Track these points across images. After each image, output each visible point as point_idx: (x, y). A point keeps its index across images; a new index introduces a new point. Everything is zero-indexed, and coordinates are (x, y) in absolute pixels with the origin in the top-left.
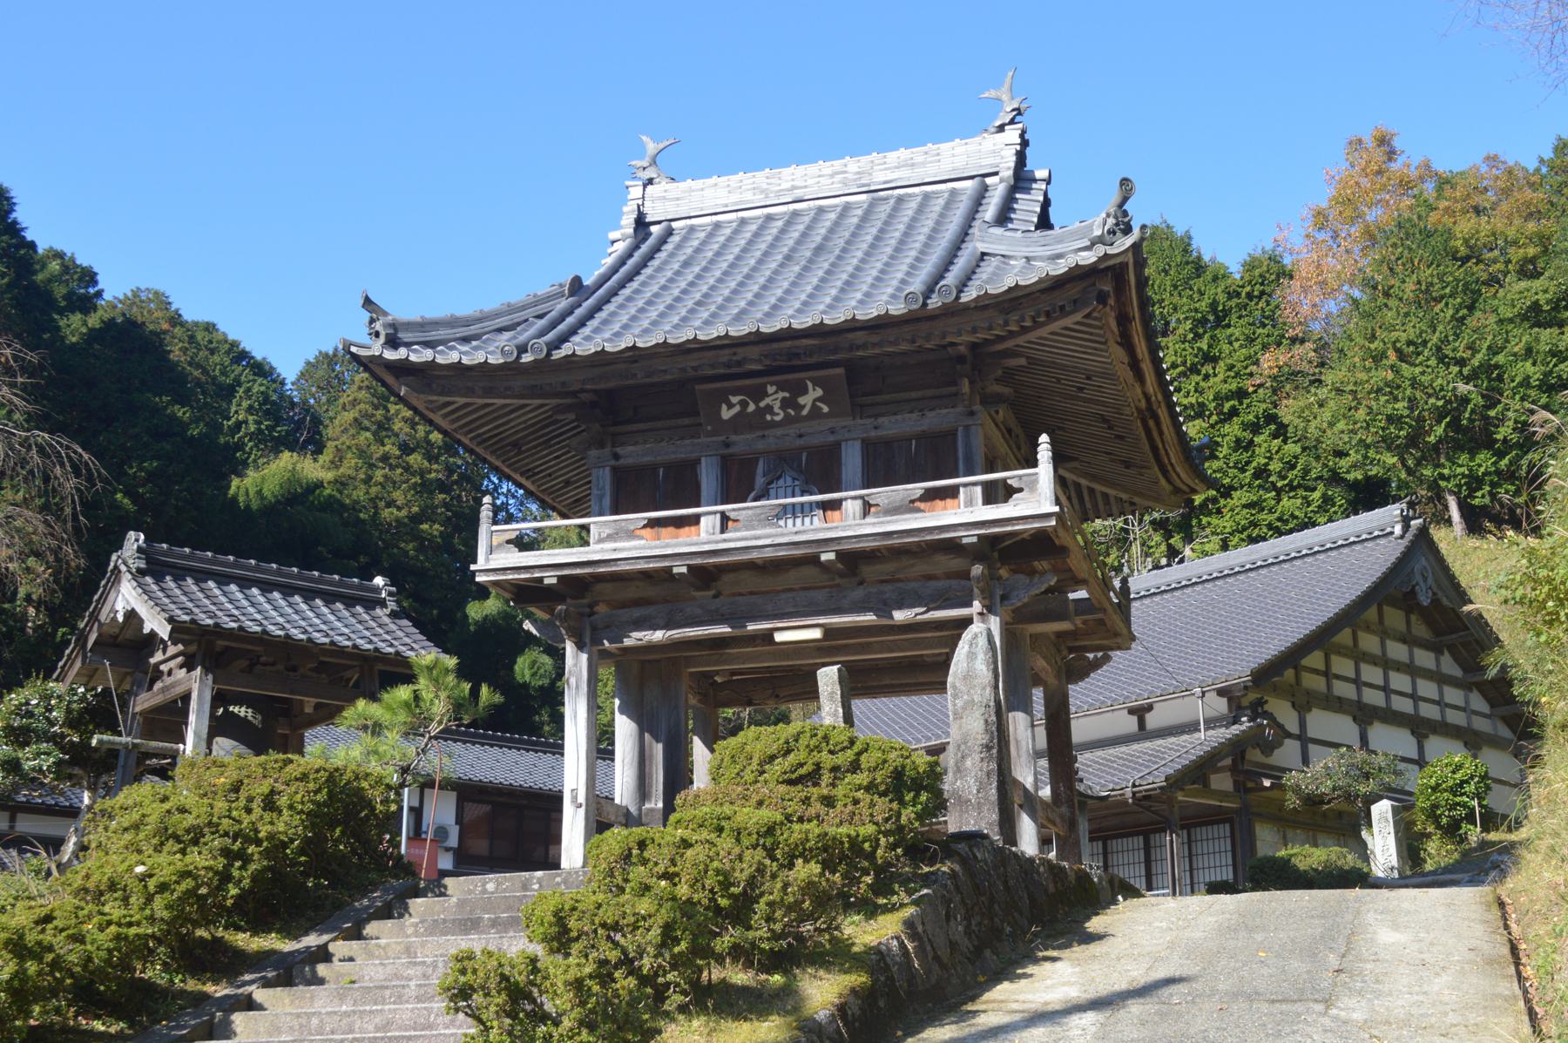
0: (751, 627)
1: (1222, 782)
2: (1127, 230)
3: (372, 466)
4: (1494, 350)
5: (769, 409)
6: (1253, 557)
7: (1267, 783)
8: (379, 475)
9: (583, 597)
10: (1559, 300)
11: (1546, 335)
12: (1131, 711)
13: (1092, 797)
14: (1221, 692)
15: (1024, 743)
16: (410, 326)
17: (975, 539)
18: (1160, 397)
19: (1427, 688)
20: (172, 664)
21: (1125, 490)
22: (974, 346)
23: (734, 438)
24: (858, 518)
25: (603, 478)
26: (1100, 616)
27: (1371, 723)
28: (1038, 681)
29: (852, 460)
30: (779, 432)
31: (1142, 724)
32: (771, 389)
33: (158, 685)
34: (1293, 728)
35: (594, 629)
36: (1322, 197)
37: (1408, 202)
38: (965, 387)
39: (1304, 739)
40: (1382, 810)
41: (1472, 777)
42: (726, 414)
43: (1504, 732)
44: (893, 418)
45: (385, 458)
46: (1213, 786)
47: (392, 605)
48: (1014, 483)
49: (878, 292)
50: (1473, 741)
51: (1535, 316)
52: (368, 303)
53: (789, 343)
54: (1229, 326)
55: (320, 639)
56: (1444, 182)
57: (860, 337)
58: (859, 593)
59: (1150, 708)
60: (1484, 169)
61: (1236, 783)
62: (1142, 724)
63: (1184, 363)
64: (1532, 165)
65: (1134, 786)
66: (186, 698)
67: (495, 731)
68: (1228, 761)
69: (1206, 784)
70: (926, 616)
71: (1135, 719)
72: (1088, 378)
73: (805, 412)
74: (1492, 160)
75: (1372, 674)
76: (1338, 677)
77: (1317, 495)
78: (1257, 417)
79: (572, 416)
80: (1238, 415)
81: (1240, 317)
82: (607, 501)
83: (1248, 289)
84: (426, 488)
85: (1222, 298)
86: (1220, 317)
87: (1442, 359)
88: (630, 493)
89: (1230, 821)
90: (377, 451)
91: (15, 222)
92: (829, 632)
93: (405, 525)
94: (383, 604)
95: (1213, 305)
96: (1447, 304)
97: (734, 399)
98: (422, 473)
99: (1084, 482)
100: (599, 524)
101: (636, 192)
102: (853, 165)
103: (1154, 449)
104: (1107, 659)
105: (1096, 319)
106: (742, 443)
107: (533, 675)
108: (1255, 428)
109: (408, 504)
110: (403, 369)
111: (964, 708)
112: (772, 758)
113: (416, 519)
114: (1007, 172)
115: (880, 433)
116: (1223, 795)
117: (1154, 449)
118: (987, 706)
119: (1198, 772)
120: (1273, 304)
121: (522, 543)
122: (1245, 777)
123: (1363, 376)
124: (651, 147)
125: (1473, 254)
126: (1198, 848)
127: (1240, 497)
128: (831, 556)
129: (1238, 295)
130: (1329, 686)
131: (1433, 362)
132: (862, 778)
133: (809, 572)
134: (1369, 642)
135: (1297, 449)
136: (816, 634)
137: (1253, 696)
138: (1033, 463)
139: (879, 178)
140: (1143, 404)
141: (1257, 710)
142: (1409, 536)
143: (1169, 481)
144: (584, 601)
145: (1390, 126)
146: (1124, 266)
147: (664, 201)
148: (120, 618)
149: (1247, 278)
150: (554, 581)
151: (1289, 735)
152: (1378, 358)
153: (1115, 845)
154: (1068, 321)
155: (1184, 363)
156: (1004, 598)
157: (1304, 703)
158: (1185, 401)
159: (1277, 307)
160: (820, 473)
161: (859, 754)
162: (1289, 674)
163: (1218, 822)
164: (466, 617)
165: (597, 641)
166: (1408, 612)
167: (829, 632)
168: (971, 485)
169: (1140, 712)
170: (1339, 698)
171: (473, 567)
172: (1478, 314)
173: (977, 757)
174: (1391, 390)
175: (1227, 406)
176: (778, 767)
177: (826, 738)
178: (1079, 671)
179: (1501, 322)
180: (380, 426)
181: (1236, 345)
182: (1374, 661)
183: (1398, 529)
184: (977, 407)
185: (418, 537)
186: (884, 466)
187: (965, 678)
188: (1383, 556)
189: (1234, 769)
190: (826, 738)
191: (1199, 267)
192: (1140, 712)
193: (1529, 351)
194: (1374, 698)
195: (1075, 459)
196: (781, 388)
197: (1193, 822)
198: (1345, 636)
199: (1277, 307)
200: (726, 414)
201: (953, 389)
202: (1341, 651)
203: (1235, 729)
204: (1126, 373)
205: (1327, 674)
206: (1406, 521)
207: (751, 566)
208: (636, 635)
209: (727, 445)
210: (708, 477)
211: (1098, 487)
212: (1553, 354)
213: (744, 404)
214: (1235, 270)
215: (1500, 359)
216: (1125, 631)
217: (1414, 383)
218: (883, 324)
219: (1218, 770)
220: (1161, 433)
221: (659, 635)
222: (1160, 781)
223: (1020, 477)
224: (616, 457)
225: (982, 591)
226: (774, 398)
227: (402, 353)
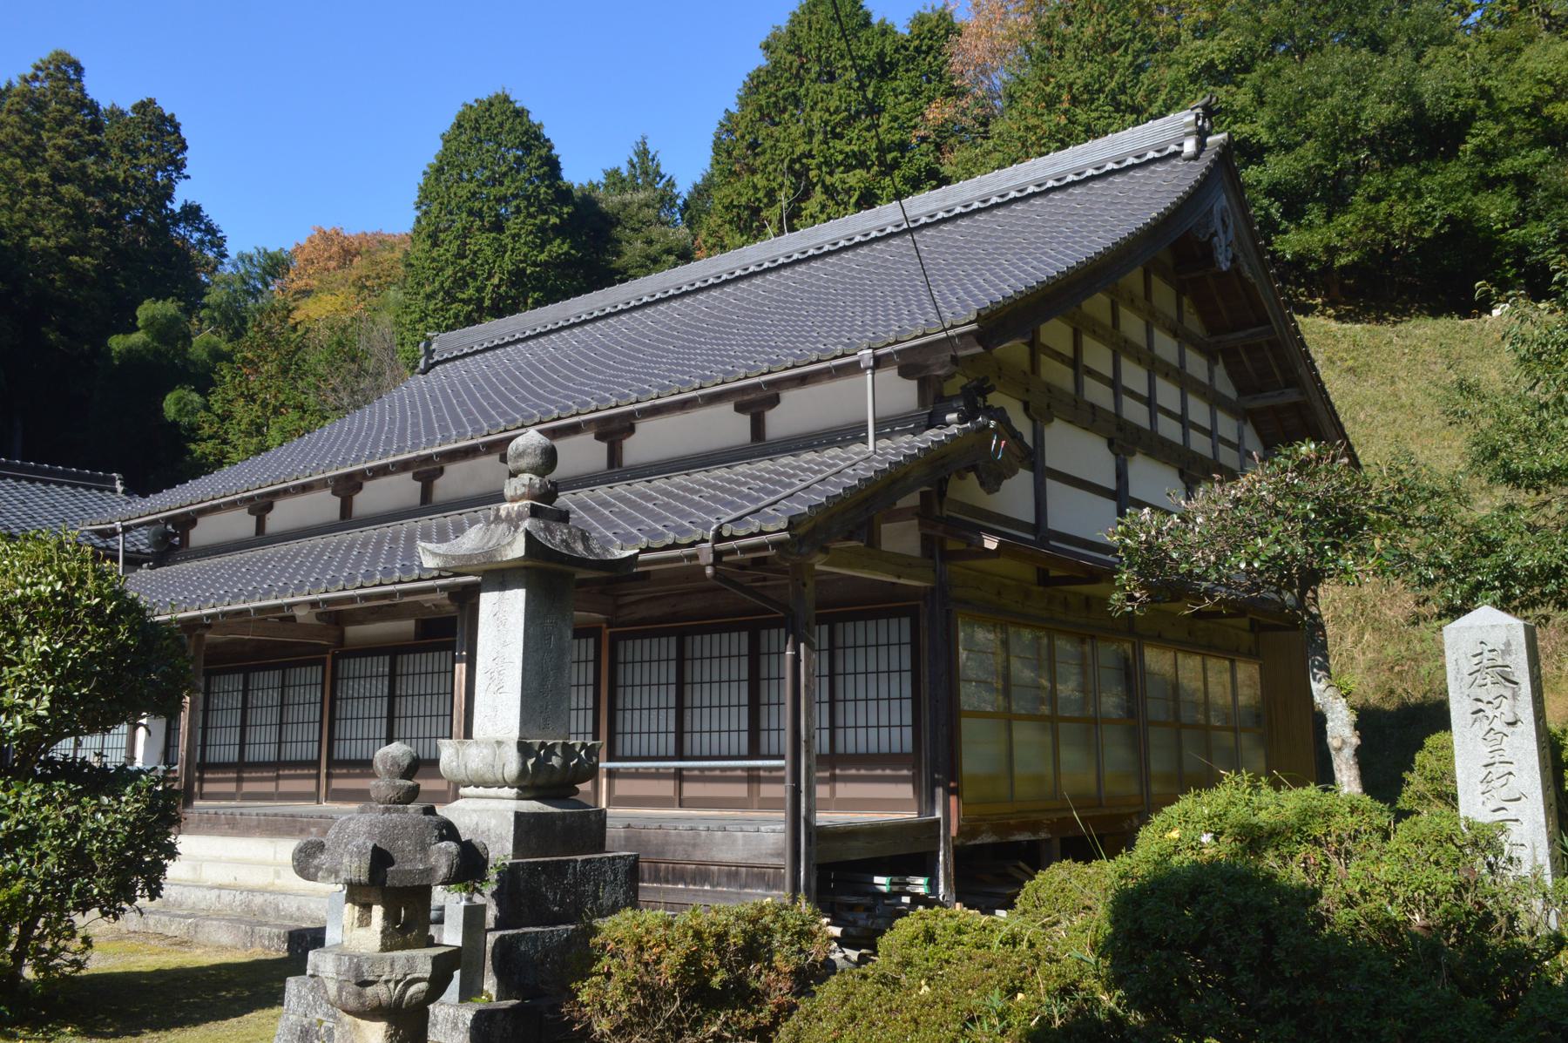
1: (901, 538)
6: (949, 203)
13: (582, 563)
19: (1199, 411)
27: (1133, 454)
31: (614, 457)
46: (886, 545)
54: (895, 79)
61: (926, 541)
63: (848, 110)
65: (719, 537)
67: (40, 461)
68: (912, 500)
69: (873, 541)
71: (746, 420)
76: (1091, 373)
78: (919, 170)
80: (899, 168)
81: (907, 71)
83: (917, 42)
86: (884, 68)
90: (23, 177)
93: (52, 255)
95: (881, 55)
96: (1126, 50)
98: (76, 204)
107: (179, 411)
109: (57, 234)
113: (66, 250)
116: (900, 563)
119: (857, 513)
120: (941, 58)
122: (948, 531)
126: (847, 662)
130: (1078, 385)
142: (1208, 157)
149: (916, 32)
155: (848, 110)
158: (847, 149)
159: (946, 62)
163: (888, 614)
164: (109, 350)
169: (755, 403)
170: (1093, 406)
175: (889, 157)
181: (902, 98)
183: (1189, 146)
185: (68, 269)
189: (924, 513)
192: (755, 403)
198: (1097, 305)
199: (946, 62)
203: (932, 435)
206: (1202, 135)
214: (902, 28)
222: (775, 526)
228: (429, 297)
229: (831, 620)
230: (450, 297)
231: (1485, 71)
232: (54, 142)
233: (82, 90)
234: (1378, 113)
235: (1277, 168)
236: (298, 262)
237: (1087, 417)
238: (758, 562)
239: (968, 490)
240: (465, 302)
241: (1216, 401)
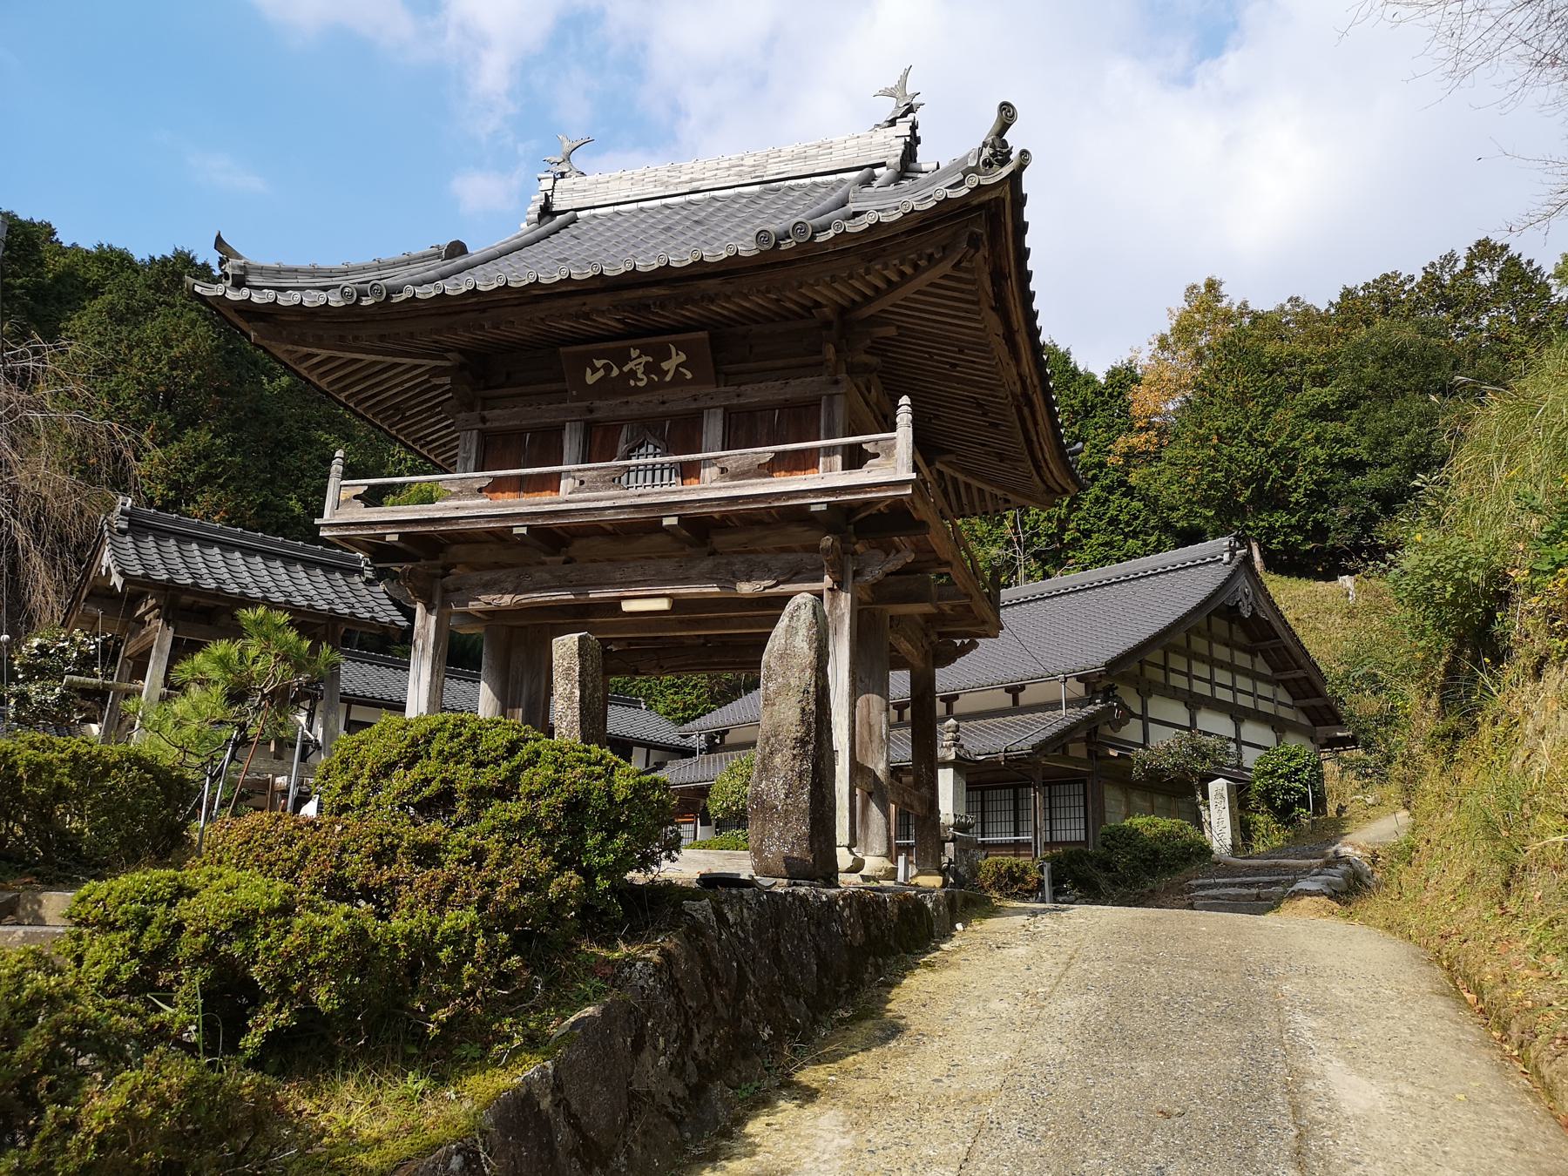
0: (595, 595)
1: (1078, 750)
2: (1005, 160)
5: (633, 373)
7: (1113, 753)
9: (437, 558)
10: (1341, 403)
12: (1008, 690)
14: (1080, 679)
15: (876, 728)
16: (261, 271)
17: (824, 507)
18: (1036, 381)
19: (1243, 683)
20: (151, 615)
21: (1001, 487)
22: (842, 311)
23: (597, 403)
26: (966, 601)
28: (898, 664)
30: (642, 398)
31: (1015, 700)
32: (634, 353)
34: (1137, 710)
35: (446, 591)
38: (830, 352)
39: (1145, 719)
40: (1218, 786)
41: (1305, 766)
42: (591, 379)
43: (1304, 720)
44: (756, 386)
47: (369, 574)
48: (869, 448)
50: (1279, 726)
51: (1322, 413)
53: (640, 292)
55: (322, 605)
56: (1257, 318)
57: (711, 285)
58: (707, 564)
59: (1023, 688)
61: (1089, 752)
62: (1015, 700)
68: (1084, 734)
69: (1065, 751)
70: (774, 590)
72: (961, 351)
73: (668, 379)
74: (1294, 300)
76: (1173, 671)
77: (1153, 538)
79: (447, 380)
85: (1090, 397)
86: (1088, 411)
87: (1251, 443)
89: (1084, 782)
92: (678, 603)
94: (361, 572)
97: (598, 363)
99: (961, 477)
103: (1029, 441)
104: (974, 645)
105: (967, 270)
106: (605, 408)
108: (1110, 490)
111: (778, 694)
112: (389, 768)
114: (894, 160)
115: (742, 401)
116: (1077, 761)
117: (1029, 441)
118: (806, 691)
123: (1190, 452)
125: (1275, 368)
126: (1057, 802)
127: (1097, 538)
128: (674, 521)
129: (1102, 394)
131: (1245, 444)
132: (515, 810)
133: (658, 539)
134: (1200, 645)
135: (1140, 505)
136: (663, 604)
137: (1105, 683)
138: (893, 427)
140: (1018, 389)
141: (1108, 693)
143: (1044, 481)
144: (439, 562)
146: (999, 201)
150: (395, 538)
151: (1134, 715)
152: (1205, 440)
153: (990, 794)
154: (933, 275)
156: (856, 574)
157: (1146, 690)
160: (679, 435)
161: (520, 768)
162: (1135, 666)
163: (1075, 782)
165: (445, 604)
166: (1231, 622)
167: (678, 603)
171: (317, 521)
172: (1280, 410)
173: (788, 753)
174: (1213, 464)
175: (1090, 474)
176: (400, 780)
177: (474, 739)
178: (948, 656)
182: (1202, 659)
183: (1226, 557)
184: (842, 376)
187: (781, 657)
188: (1203, 584)
190: (474, 739)
191: (1075, 373)
192: (1015, 691)
193: (1317, 439)
194: (1202, 688)
195: (950, 452)
196: (644, 352)
197: (1053, 782)
200: (591, 379)
201: (818, 358)
202: (1177, 650)
203: (1090, 709)
204: (1002, 350)
206: (1232, 551)
208: (484, 598)
209: (591, 411)
211: (975, 484)
213: (608, 368)
214: (1101, 378)
215: (1297, 443)
216: (993, 618)
217: (1231, 459)
218: (733, 268)
219: (1074, 741)
220: (1036, 424)
221: (507, 600)
223: (876, 441)
224: (484, 420)
225: (832, 565)
226: (638, 362)
227: (244, 293)
229: (1049, 785)
237: (1173, 693)
238: (1019, 760)
239: (1107, 731)
241: (1255, 676)
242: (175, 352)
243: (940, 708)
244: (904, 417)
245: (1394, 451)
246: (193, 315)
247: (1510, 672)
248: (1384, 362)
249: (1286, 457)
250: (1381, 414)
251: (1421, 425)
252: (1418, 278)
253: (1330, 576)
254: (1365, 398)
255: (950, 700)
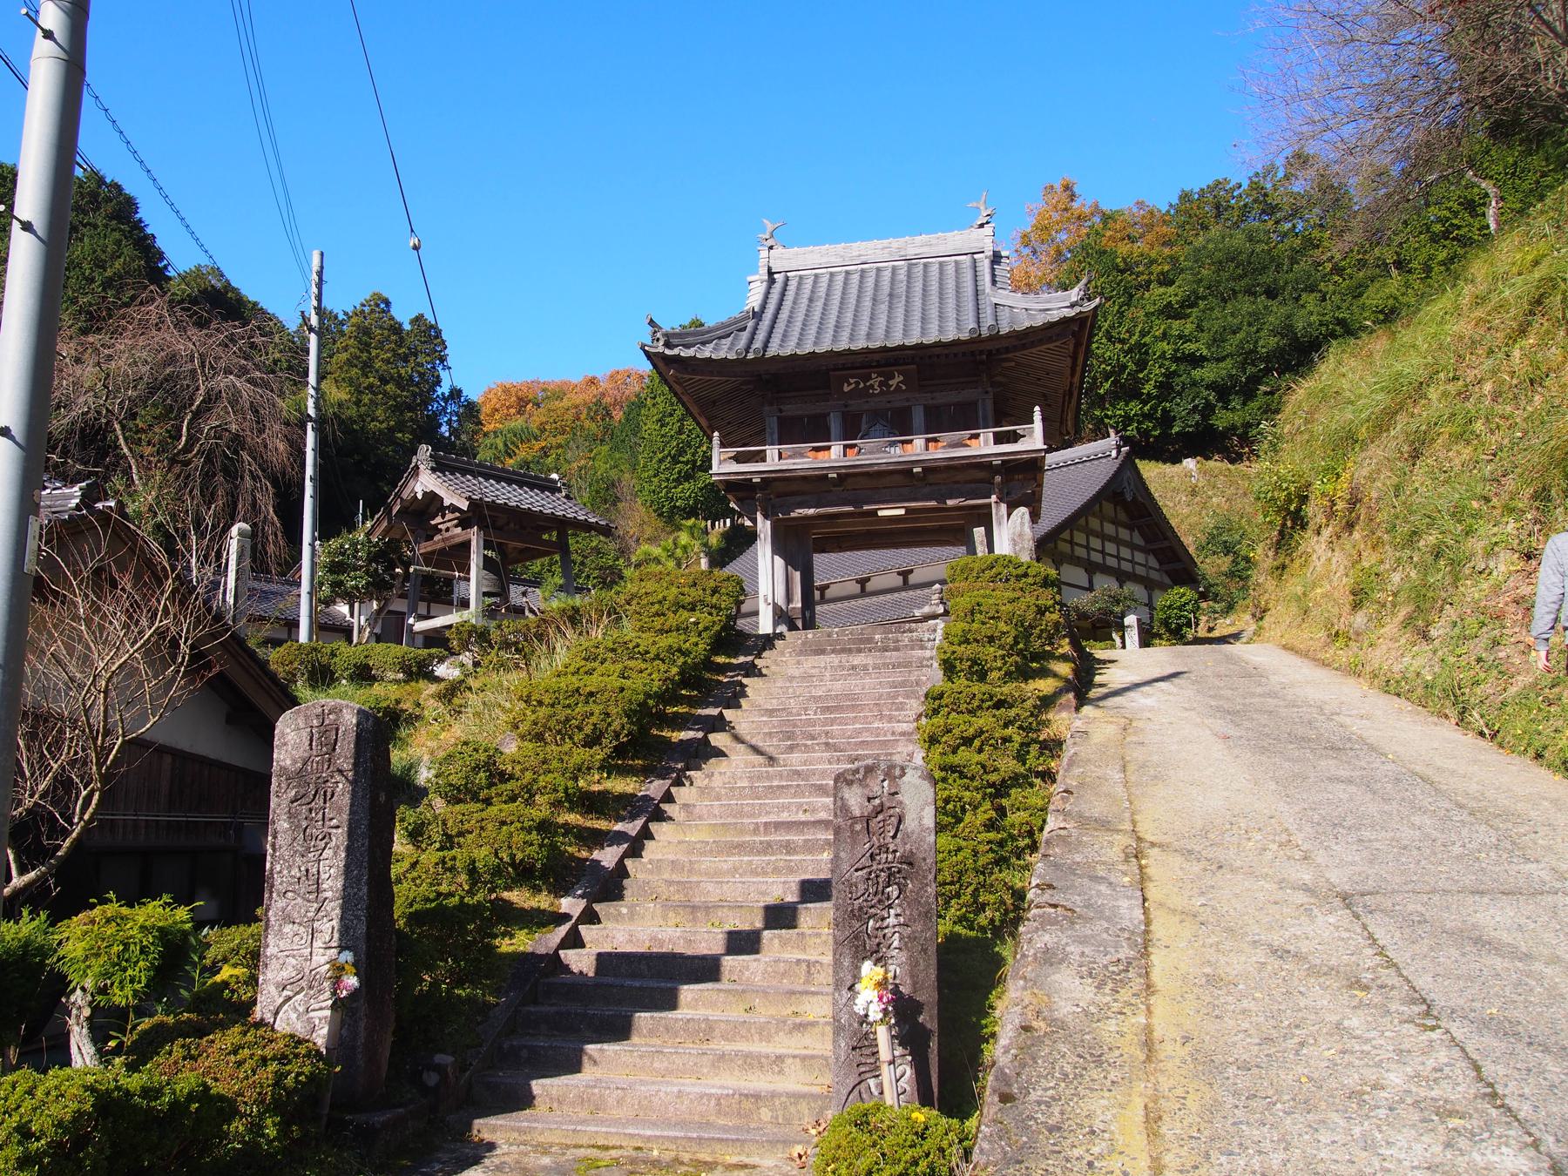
3: (360, 392)
4: (1143, 334)
5: (872, 386)
8: (366, 399)
11: (1176, 324)
12: (858, 581)
16: (675, 335)
19: (1125, 553)
24: (917, 449)
25: (772, 424)
29: (918, 417)
31: (905, 581)
33: (436, 538)
36: (1027, 224)
37: (1084, 231)
42: (846, 388)
45: (370, 387)
49: (950, 327)
51: (1169, 312)
52: (652, 323)
56: (1107, 218)
58: (926, 490)
60: (1135, 210)
64: (1164, 209)
66: (469, 542)
74: (1140, 204)
75: (1095, 543)
82: (776, 436)
84: (399, 408)
88: (790, 433)
91: (140, 221)
92: (908, 510)
100: (772, 451)
101: (764, 253)
102: (895, 243)
110: (677, 359)
113: (391, 430)
121: (738, 459)
124: (770, 227)
125: (1128, 268)
134: (1094, 523)
136: (902, 512)
138: (1032, 422)
139: (911, 252)
142: (1121, 457)
145: (1072, 178)
147: (785, 259)
148: (420, 496)
154: (1051, 346)
160: (900, 426)
167: (908, 510)
168: (987, 435)
179: (1146, 315)
180: (365, 363)
183: (1114, 453)
185: (393, 442)
186: (937, 423)
188: (1101, 474)
192: (863, 582)
193: (1165, 336)
194: (1096, 557)
200: (846, 388)
205: (1071, 542)
206: (1118, 448)
207: (867, 474)
210: (835, 424)
212: (1180, 337)
213: (857, 383)
215: (1147, 339)
221: (811, 511)
226: (875, 381)
228: (661, 461)
230: (675, 461)
231: (1339, 308)
232: (380, 357)
233: (392, 318)
234: (1269, 343)
235: (1207, 373)
236: (486, 410)
240: (687, 463)
241: (1133, 547)
242: (109, 273)
243: (817, 593)
244: (1037, 416)
245: (1228, 349)
246: (117, 235)
247: (1309, 533)
248: (1220, 265)
249: (1141, 354)
250: (1216, 313)
251: (1250, 324)
252: (1245, 185)
253: (1176, 460)
254: (1204, 298)
255: (823, 589)
